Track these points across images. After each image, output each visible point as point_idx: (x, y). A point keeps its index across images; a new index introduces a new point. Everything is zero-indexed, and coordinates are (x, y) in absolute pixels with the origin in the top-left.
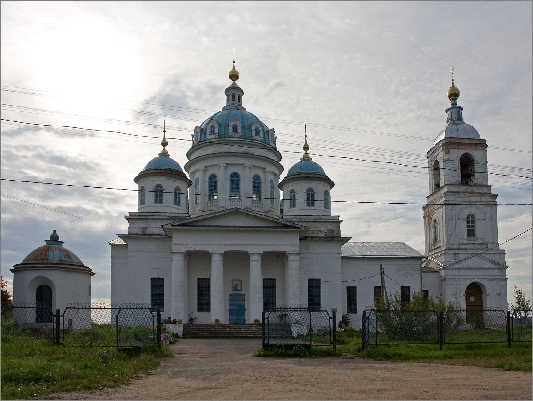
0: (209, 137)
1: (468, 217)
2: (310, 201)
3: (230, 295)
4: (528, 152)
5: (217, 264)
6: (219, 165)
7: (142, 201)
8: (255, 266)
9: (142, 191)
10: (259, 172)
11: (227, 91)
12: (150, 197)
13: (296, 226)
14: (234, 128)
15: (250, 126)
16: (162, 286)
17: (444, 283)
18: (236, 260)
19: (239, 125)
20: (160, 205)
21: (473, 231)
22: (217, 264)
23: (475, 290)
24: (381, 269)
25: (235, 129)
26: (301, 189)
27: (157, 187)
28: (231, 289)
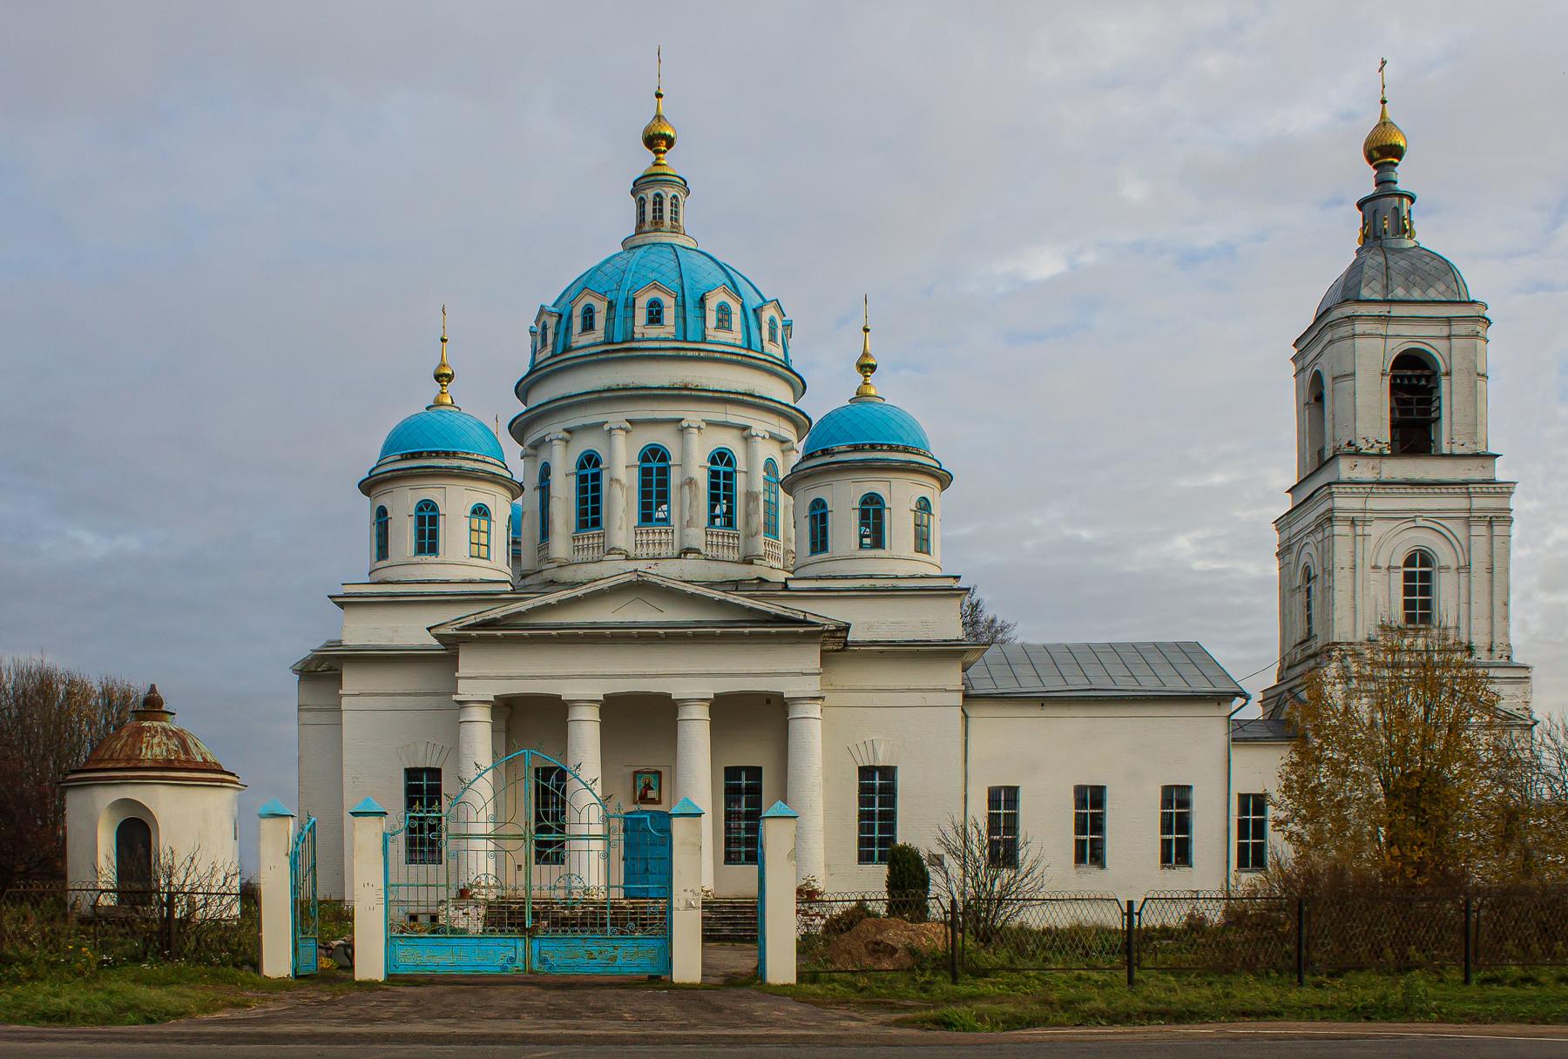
1: (1410, 561)
5: (586, 735)
6: (606, 427)
8: (696, 732)
11: (638, 186)
13: (810, 618)
14: (650, 313)
15: (702, 300)
19: (669, 303)
20: (431, 558)
21: (1426, 605)
22: (586, 735)
25: (655, 317)
27: (421, 509)
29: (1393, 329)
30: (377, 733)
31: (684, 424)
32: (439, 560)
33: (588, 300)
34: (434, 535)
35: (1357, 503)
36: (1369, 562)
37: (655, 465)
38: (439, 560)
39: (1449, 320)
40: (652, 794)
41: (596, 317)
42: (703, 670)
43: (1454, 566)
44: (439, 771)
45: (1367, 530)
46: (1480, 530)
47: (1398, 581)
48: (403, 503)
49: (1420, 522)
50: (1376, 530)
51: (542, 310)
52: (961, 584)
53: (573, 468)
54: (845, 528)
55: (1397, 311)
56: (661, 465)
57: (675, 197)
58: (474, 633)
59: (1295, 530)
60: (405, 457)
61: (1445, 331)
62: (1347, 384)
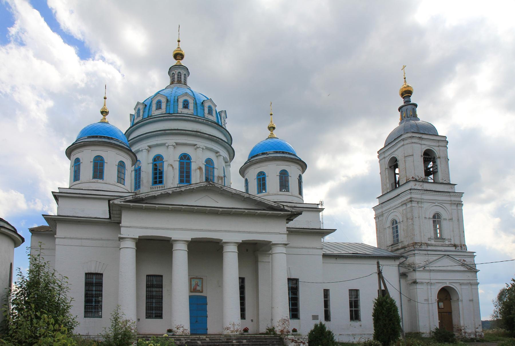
0: (155, 112)
1: (434, 217)
2: (284, 185)
3: (190, 297)
4: (285, 234)
5: (180, 256)
7: (76, 175)
10: (212, 156)
13: (286, 208)
14: (184, 104)
16: (100, 284)
17: (415, 286)
18: (205, 252)
22: (180, 256)
23: (446, 295)
24: (379, 267)
25: (186, 105)
26: (272, 171)
31: (167, 145)
35: (418, 196)
36: (423, 216)
37: (185, 161)
38: (104, 181)
40: (198, 288)
41: (162, 104)
42: (237, 229)
44: (102, 274)
45: (422, 205)
47: (431, 222)
48: (87, 156)
49: (437, 204)
51: (138, 103)
54: (273, 183)
56: (188, 161)
57: (185, 74)
58: (132, 204)
59: (384, 209)
61: (437, 145)
62: (410, 159)
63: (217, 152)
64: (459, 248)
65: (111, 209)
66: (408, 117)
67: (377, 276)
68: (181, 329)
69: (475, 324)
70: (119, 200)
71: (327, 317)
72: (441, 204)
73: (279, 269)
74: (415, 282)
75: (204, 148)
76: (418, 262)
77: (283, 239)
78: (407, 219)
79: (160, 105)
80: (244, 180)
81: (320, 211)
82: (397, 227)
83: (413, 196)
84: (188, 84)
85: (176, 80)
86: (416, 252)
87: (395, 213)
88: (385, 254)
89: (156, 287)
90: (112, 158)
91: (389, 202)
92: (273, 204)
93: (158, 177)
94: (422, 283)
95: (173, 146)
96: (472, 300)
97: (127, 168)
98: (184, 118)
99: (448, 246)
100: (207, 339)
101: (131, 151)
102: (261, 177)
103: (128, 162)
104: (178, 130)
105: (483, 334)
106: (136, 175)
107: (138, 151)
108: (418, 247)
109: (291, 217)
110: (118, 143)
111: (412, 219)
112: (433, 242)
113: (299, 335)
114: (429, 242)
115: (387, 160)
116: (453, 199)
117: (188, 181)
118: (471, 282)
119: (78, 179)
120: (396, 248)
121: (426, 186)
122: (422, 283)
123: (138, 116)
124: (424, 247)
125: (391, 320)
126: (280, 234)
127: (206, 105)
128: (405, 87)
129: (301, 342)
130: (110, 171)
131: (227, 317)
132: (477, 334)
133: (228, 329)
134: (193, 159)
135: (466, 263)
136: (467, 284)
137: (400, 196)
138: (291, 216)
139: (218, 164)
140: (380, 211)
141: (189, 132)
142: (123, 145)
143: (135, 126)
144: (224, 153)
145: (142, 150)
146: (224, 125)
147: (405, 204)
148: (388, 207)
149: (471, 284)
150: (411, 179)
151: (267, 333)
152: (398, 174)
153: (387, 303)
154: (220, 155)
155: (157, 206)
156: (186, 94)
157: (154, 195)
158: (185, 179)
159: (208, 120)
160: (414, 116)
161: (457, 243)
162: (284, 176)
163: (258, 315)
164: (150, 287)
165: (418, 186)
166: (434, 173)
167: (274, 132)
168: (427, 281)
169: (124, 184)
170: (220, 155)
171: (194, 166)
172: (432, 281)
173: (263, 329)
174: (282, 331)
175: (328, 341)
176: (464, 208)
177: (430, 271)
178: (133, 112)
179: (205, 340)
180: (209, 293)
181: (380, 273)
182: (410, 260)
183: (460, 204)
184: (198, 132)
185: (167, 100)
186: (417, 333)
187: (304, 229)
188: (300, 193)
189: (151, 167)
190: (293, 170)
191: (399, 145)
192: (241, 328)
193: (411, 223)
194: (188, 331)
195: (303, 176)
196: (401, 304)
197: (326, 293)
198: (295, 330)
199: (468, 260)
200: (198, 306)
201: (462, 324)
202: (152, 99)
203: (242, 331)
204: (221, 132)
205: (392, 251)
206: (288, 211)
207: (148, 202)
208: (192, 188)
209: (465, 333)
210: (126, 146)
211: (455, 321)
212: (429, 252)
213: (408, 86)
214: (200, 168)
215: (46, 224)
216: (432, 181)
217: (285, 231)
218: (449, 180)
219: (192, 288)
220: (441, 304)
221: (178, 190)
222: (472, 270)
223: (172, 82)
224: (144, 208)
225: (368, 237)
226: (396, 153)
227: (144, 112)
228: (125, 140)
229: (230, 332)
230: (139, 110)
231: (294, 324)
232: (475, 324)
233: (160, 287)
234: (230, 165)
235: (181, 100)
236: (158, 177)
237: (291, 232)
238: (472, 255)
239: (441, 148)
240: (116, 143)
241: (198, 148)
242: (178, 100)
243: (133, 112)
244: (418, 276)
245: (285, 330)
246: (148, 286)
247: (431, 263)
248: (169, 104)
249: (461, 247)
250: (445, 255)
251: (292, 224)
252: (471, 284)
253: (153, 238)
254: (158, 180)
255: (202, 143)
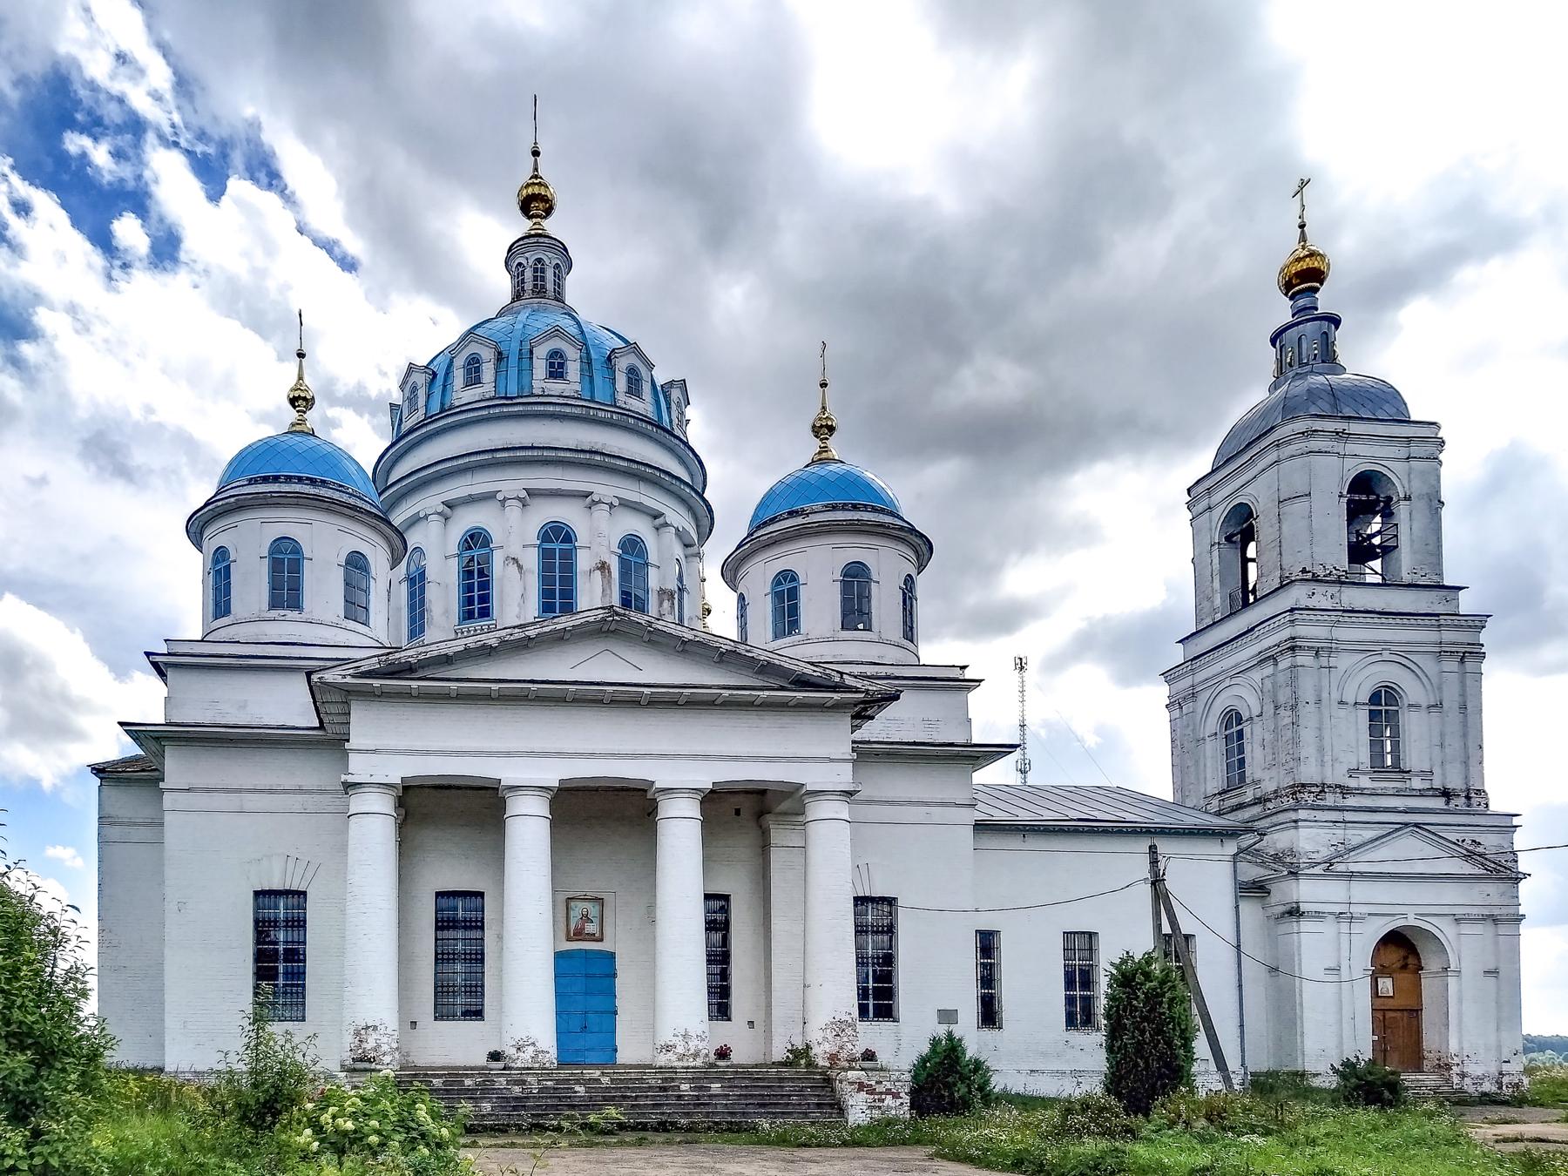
0: (462, 395)
1: (1375, 698)
3: (560, 957)
5: (528, 830)
7: (220, 602)
9: (220, 573)
12: (252, 587)
13: (849, 681)
14: (552, 365)
17: (1292, 925)
18: (606, 815)
19: (572, 354)
20: (291, 614)
22: (528, 830)
24: (1154, 862)
25: (556, 369)
26: (819, 566)
28: (563, 935)
29: (1351, 448)
30: (227, 839)
31: (500, 496)
32: (304, 616)
33: (473, 348)
34: (794, 611)
36: (1335, 696)
37: (557, 546)
38: (304, 616)
39: (1409, 439)
40: (591, 928)
43: (1424, 705)
44: (304, 893)
45: (1333, 662)
46: (1451, 665)
47: (1363, 715)
48: (250, 539)
49: (1386, 656)
50: (1343, 662)
51: (411, 368)
52: (968, 674)
53: (453, 549)
54: (820, 604)
55: (1355, 428)
56: (566, 546)
58: (376, 683)
60: (252, 482)
61: (1403, 453)
62: (1299, 507)
63: (656, 515)
64: (1460, 802)
65: (318, 697)
66: (1301, 364)
67: (1147, 889)
68: (530, 1050)
69: (1499, 1048)
70: (337, 671)
71: (989, 1014)
72: (1404, 657)
73: (827, 865)
74: (1295, 912)
75: (616, 502)
76: (1308, 848)
77: (842, 776)
78: (1276, 708)
79: (478, 370)
80: (734, 596)
81: (969, 689)
82: (1240, 734)
83: (1301, 630)
84: (570, 298)
85: (529, 286)
86: (1302, 814)
87: (1235, 691)
88: (1190, 820)
89: (465, 928)
90: (326, 543)
91: (1216, 654)
92: (809, 670)
93: (477, 598)
94: (1319, 915)
95: (518, 498)
96: (1493, 973)
97: (373, 573)
98: (551, 408)
99: (1422, 794)
100: (605, 1080)
101: (389, 523)
102: (786, 586)
103: (377, 555)
104: (532, 448)
105: (1526, 1081)
106: (412, 595)
107: (415, 520)
108: (1310, 799)
109: (865, 709)
110: (345, 498)
111: (1294, 708)
112: (1365, 782)
113: (882, 1070)
114: (1352, 783)
115: (1219, 514)
116: (1448, 636)
117: (568, 608)
118: (1496, 912)
119: (227, 612)
120: (1235, 801)
121: (1353, 597)
122: (1319, 915)
123: (413, 409)
124: (1330, 799)
125: (1159, 1031)
126: (832, 760)
127: (622, 364)
128: (1299, 260)
129: (888, 1092)
130: (323, 587)
131: (666, 1017)
132: (1505, 1080)
133: (668, 1048)
134: (497, 538)
135: (1480, 850)
136: (1484, 918)
137: (1256, 633)
138: (863, 711)
139: (662, 551)
140: (1185, 683)
141: (568, 454)
142: (359, 503)
143: (404, 441)
144: (677, 516)
145: (426, 517)
146: (680, 425)
147: (1273, 658)
148: (1216, 669)
149: (1495, 920)
150: (1296, 573)
151: (785, 1064)
152: (1253, 560)
153: (1148, 976)
154: (666, 525)
155: (453, 685)
156: (557, 332)
157: (443, 652)
158: (558, 601)
159: (627, 413)
160: (1328, 356)
161: (1455, 783)
162: (855, 581)
163: (769, 1006)
164: (448, 928)
165: (1322, 597)
166: (1386, 551)
167: (832, 443)
168: (1337, 909)
169: (366, 624)
170: (666, 525)
171: (583, 561)
172: (1355, 909)
173: (779, 1053)
174: (833, 1058)
175: (970, 1092)
176: (1485, 666)
177: (1351, 876)
178: (397, 397)
179: (597, 1081)
180: (619, 940)
181: (1157, 882)
182: (1279, 840)
183: (1472, 654)
184: (596, 452)
185: (500, 353)
186: (1296, 1074)
187: (915, 743)
188: (909, 632)
189: (453, 567)
190: (887, 564)
191: (1261, 465)
192: (709, 1048)
193: (1288, 721)
194: (553, 1054)
195: (921, 581)
196: (1240, 980)
197: (987, 943)
198: (869, 1056)
199: (1489, 842)
200: (586, 981)
201: (1453, 1047)
202: (452, 352)
203: (712, 1057)
204: (671, 450)
205: (1219, 814)
206: (857, 691)
207: (428, 673)
208: (559, 627)
209: (1463, 1075)
210: (377, 505)
211: (1430, 1040)
212: (1349, 816)
213: (1312, 254)
214: (603, 567)
215: (135, 750)
216: (1378, 579)
217: (845, 750)
218: (1440, 574)
219: (572, 927)
220: (1386, 985)
221: (517, 636)
222: (1505, 872)
223: (517, 296)
224: (414, 693)
225: (1148, 770)
226: (1248, 490)
227: (428, 396)
228: (371, 491)
229: (674, 1058)
230: (414, 389)
231: (874, 1035)
232: (1499, 1048)
233: (476, 928)
234: (698, 555)
235: (541, 352)
236: (477, 598)
237: (866, 755)
238: (1506, 825)
239: (1413, 463)
240: (336, 495)
241: (595, 503)
242: (531, 352)
243: (397, 397)
244: (1306, 891)
245: (843, 1055)
246: (441, 925)
247: (1354, 849)
248: (503, 364)
249: (1468, 798)
250: (1406, 825)
251: (879, 728)
252: (1495, 920)
253: (453, 783)
254: (476, 606)
255: (606, 487)
